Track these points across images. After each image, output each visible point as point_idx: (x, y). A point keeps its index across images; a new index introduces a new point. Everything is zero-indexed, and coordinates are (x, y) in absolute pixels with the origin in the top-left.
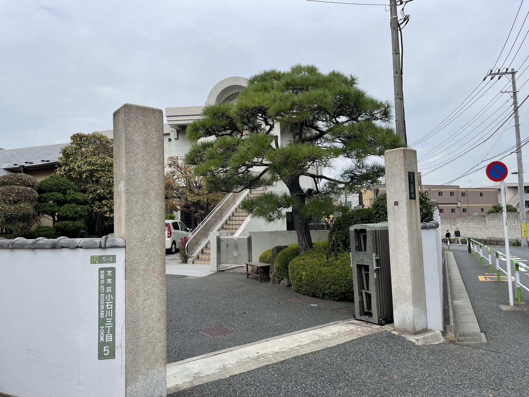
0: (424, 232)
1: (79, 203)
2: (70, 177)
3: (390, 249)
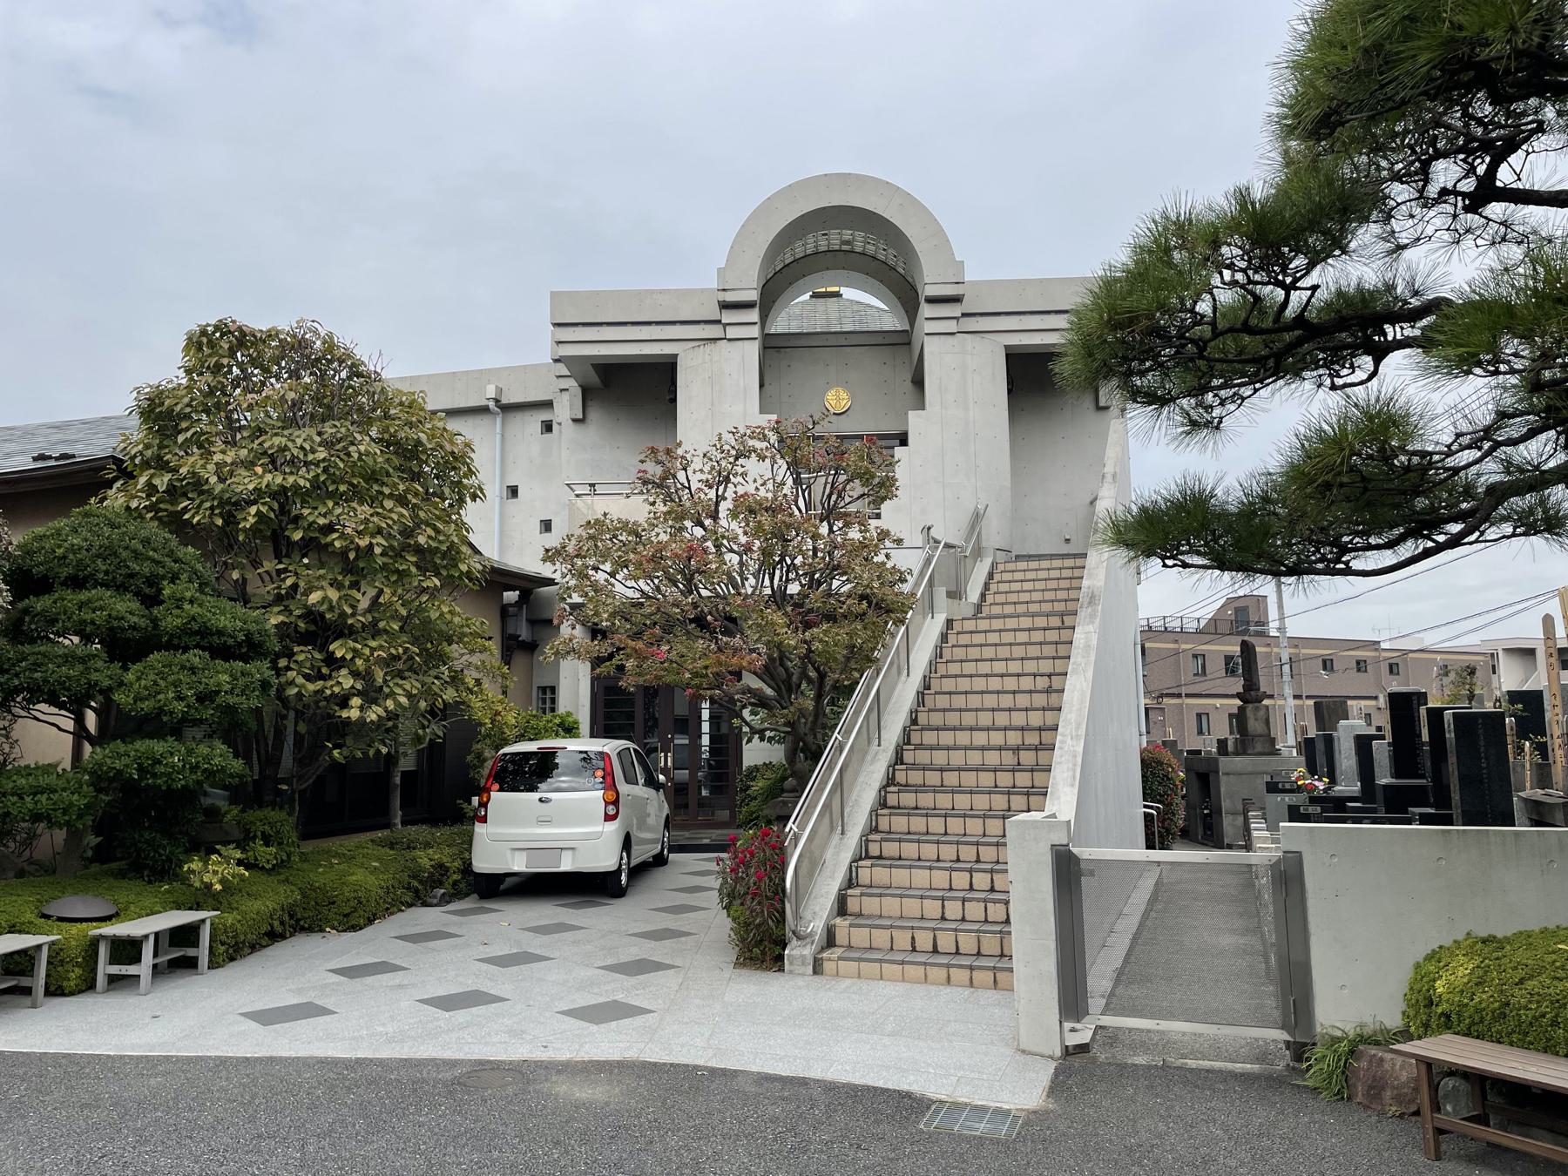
1: (223, 649)
2: (176, 523)
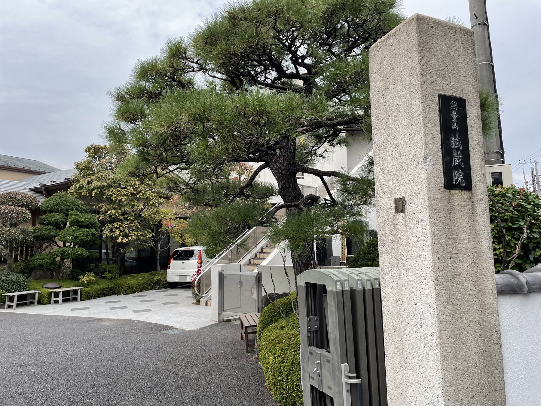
0: (509, 309)
3: (387, 359)
